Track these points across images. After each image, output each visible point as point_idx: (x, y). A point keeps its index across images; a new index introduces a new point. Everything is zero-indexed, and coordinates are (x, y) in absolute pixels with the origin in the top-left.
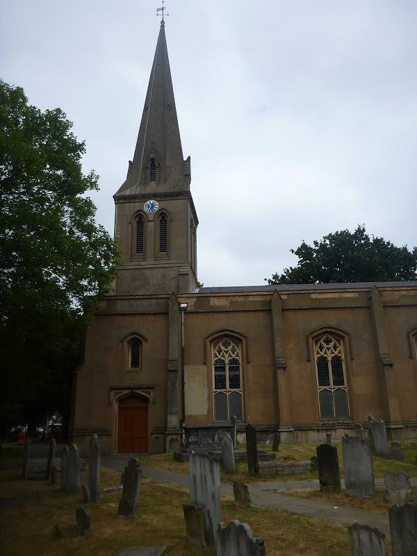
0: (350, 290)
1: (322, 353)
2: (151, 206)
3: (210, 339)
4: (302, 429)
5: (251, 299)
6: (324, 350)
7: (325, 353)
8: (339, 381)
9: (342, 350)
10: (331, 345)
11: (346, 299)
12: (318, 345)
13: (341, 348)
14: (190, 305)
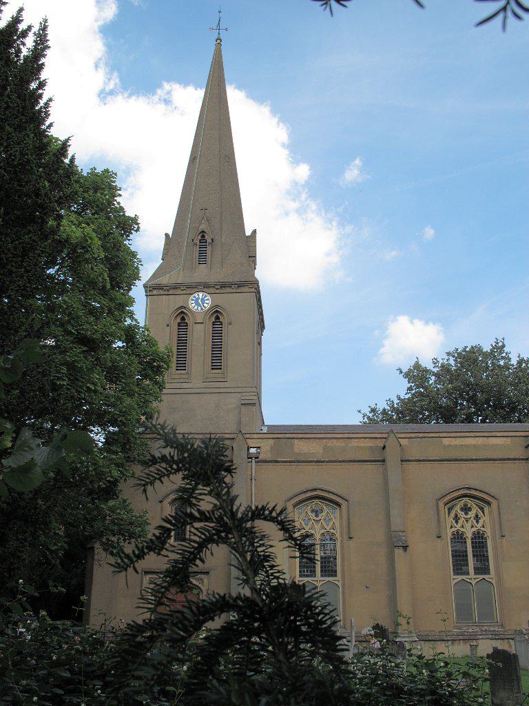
0: (498, 434)
1: (458, 526)
2: (200, 303)
3: (446, 499)
4: (427, 638)
5: (354, 443)
6: (460, 522)
7: (463, 527)
8: (483, 569)
9: (337, 524)
10: (471, 514)
11: (495, 446)
12: (453, 514)
13: (485, 519)
14: (263, 450)
